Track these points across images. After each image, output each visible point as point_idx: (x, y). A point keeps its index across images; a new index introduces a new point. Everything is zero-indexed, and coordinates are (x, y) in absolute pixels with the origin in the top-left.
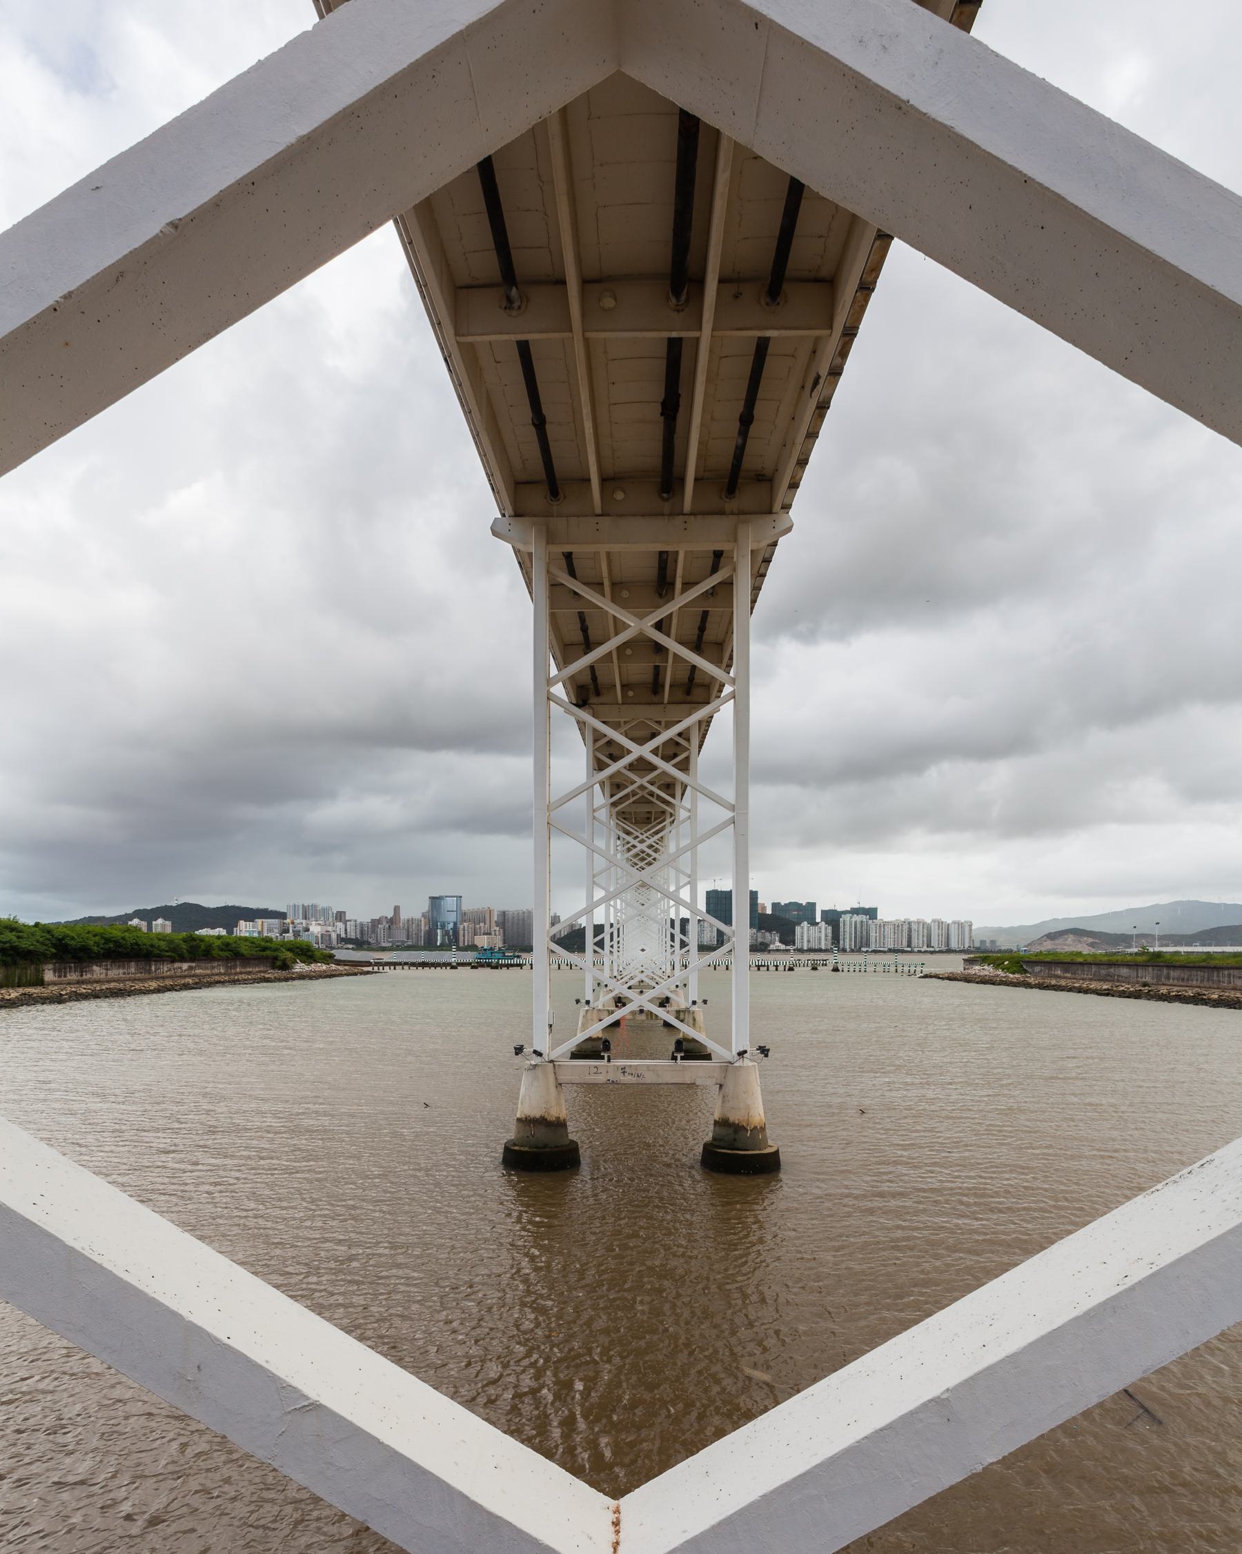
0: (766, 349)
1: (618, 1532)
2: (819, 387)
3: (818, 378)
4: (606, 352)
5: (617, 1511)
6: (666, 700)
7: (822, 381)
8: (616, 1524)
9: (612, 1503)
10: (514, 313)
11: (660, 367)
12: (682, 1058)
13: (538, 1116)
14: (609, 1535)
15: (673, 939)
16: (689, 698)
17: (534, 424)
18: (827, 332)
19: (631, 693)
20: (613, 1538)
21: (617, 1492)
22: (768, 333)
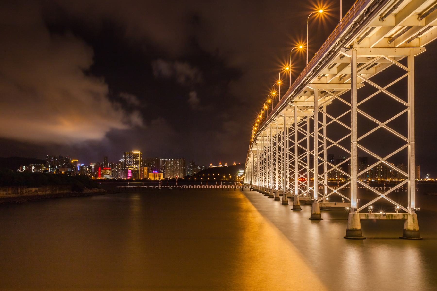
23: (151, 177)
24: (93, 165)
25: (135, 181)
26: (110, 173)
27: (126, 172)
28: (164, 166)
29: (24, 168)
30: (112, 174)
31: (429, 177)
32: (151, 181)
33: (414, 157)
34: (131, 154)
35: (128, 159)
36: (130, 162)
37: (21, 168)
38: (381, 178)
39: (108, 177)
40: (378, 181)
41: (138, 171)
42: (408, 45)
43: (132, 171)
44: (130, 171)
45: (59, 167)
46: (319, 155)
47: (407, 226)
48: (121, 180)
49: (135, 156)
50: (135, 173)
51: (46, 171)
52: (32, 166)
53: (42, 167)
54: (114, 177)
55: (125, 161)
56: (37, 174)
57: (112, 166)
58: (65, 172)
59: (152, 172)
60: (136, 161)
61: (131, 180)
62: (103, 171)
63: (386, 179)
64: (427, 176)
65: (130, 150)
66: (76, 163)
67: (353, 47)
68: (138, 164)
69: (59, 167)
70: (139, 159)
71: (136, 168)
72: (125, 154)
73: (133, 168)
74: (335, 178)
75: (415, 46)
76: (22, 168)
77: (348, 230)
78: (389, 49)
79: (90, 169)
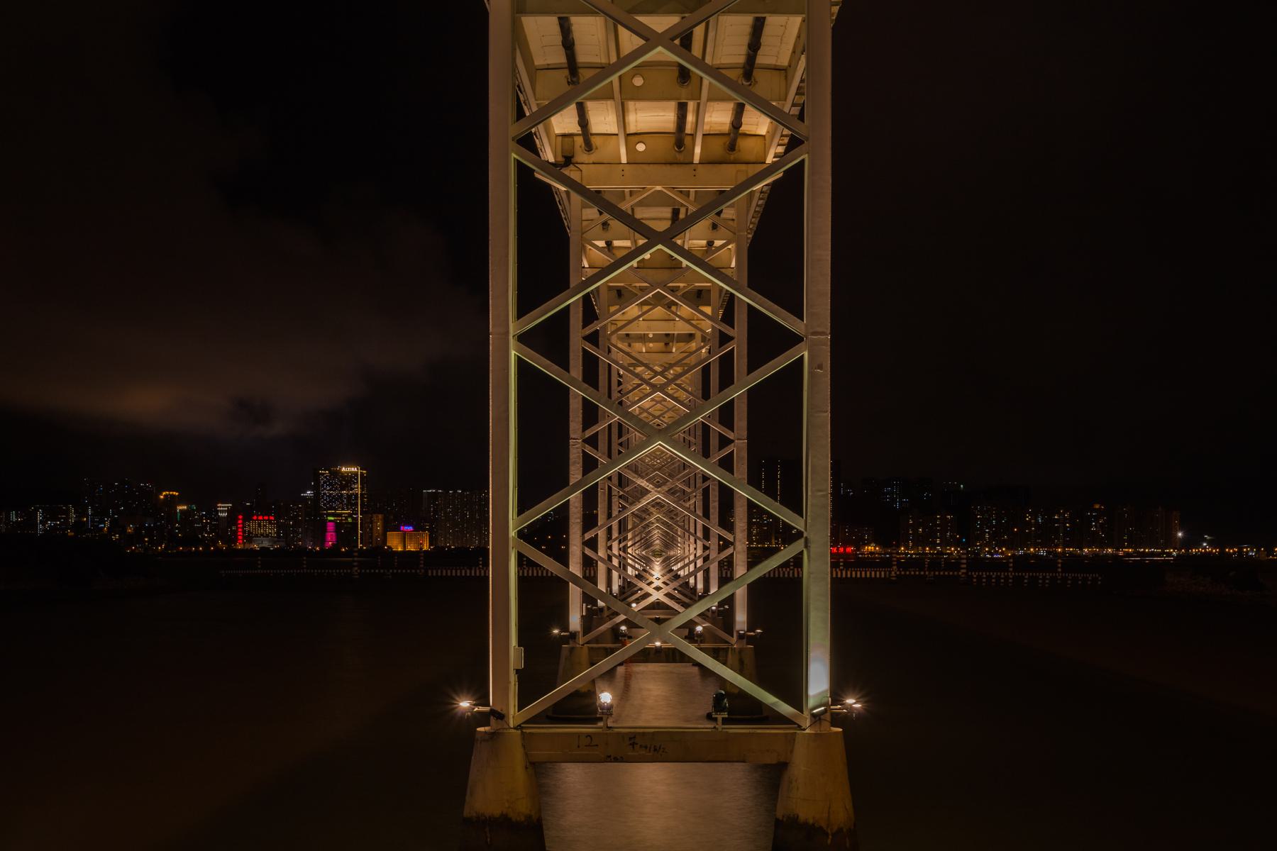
23: (395, 543)
24: (223, 509)
25: (346, 554)
26: (271, 530)
28: (435, 512)
30: (278, 533)
31: (1210, 543)
32: (392, 553)
33: (745, 466)
34: (336, 474)
35: (327, 491)
36: (333, 499)
38: (1066, 545)
39: (266, 544)
40: (1056, 554)
41: (355, 524)
42: (732, 157)
43: (338, 526)
44: (331, 527)
48: (302, 551)
49: (349, 481)
50: (346, 532)
52: (36, 510)
53: (67, 512)
54: (283, 544)
55: (317, 495)
56: (405, 554)
57: (978, 554)
58: (135, 529)
59: (397, 529)
60: (349, 497)
61: (335, 550)
62: (252, 526)
63: (1081, 549)
64: (1205, 540)
66: (171, 502)
67: (574, 160)
68: (356, 504)
70: (358, 489)
71: (350, 515)
72: (316, 477)
73: (340, 515)
74: (933, 545)
75: (752, 158)
76: (8, 517)
78: (675, 168)
79: (212, 519)
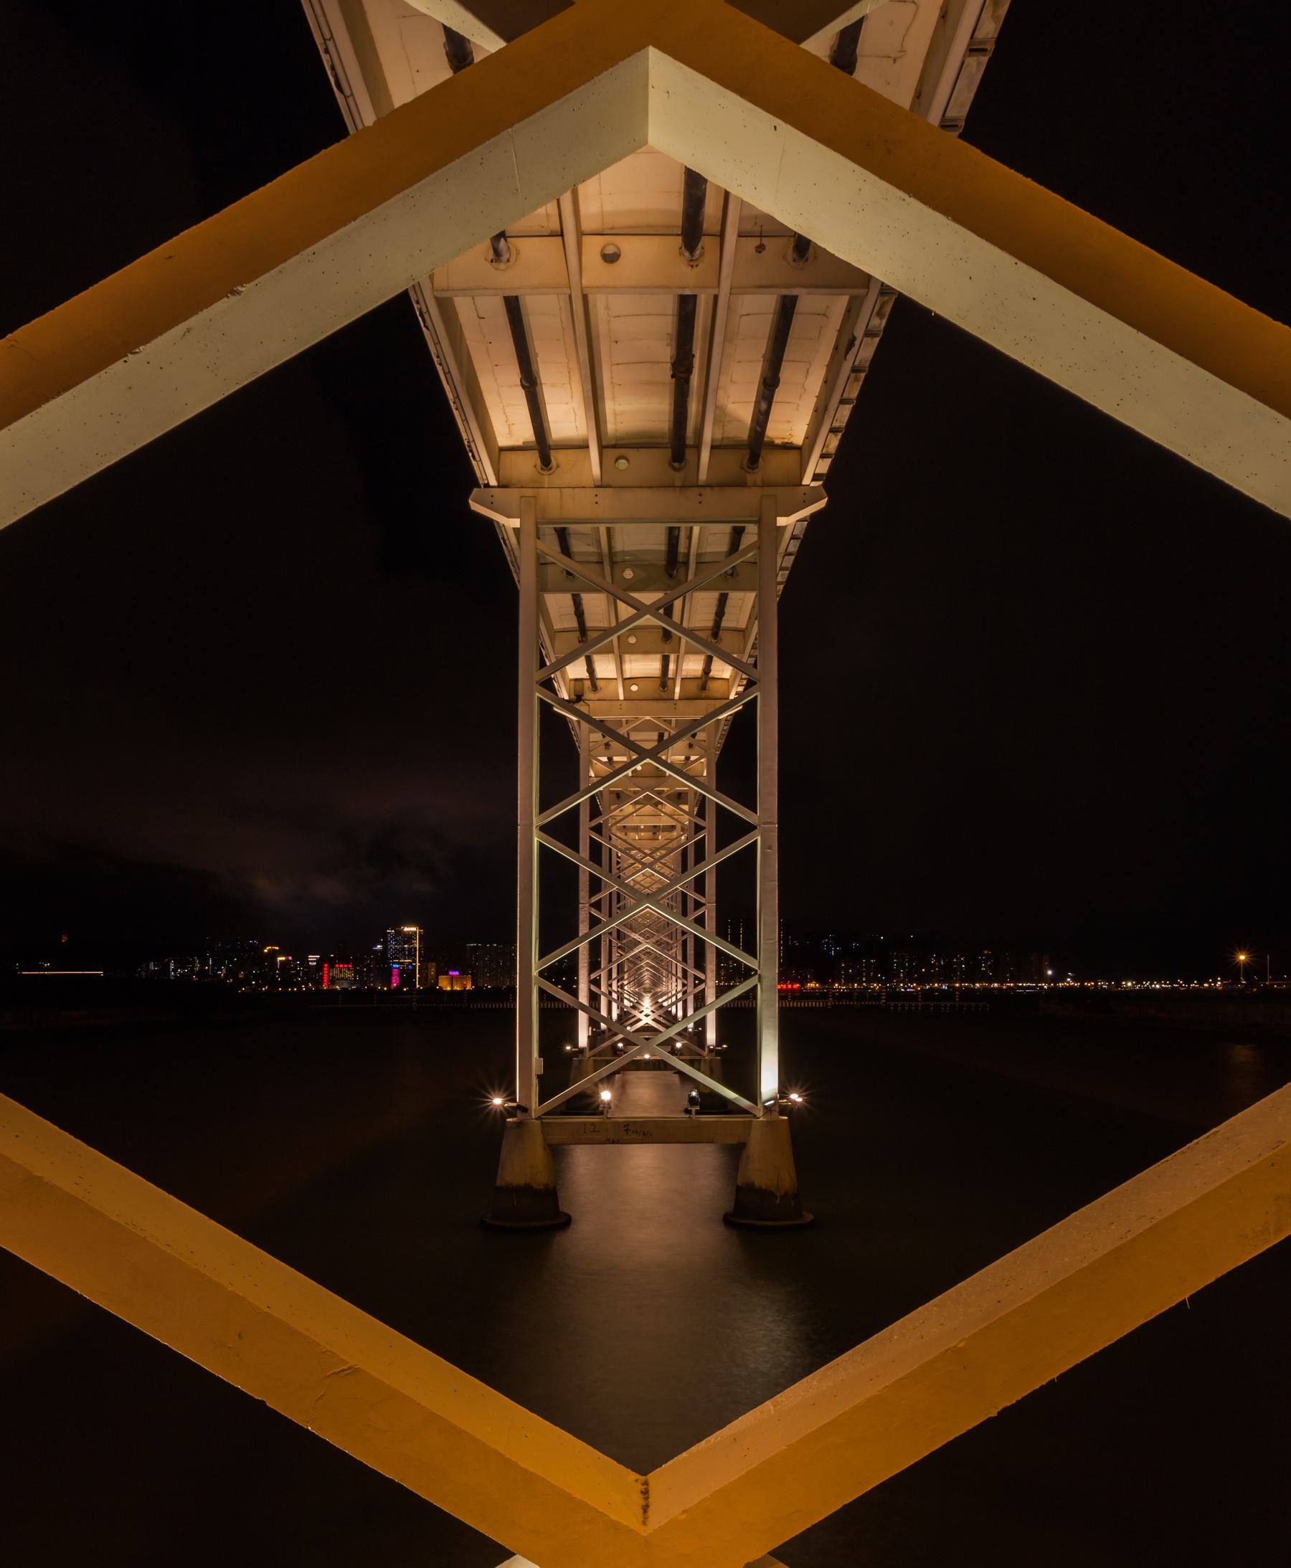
0: (794, 306)
1: (647, 1499)
2: (854, 349)
3: (853, 340)
4: (607, 308)
5: (646, 1483)
6: (677, 697)
7: (857, 343)
8: (645, 1509)
9: (642, 1478)
10: (502, 266)
11: (668, 324)
12: (698, 1113)
13: (522, 1183)
14: (639, 1500)
15: (596, 849)
16: (704, 694)
17: (523, 386)
18: (864, 291)
19: (634, 688)
20: (643, 1502)
21: (644, 1473)
22: (794, 292)
23: (444, 984)
24: (313, 959)
27: (386, 975)
29: (152, 966)
31: (1074, 979)
34: (399, 933)
35: (393, 945)
37: (144, 966)
44: (395, 972)
45: (233, 963)
46: (592, 829)
47: (979, 64)
49: (410, 937)
51: (202, 973)
53: (193, 963)
55: (385, 949)
65: (396, 925)
66: (273, 954)
69: (233, 963)
77: (739, 1190)
